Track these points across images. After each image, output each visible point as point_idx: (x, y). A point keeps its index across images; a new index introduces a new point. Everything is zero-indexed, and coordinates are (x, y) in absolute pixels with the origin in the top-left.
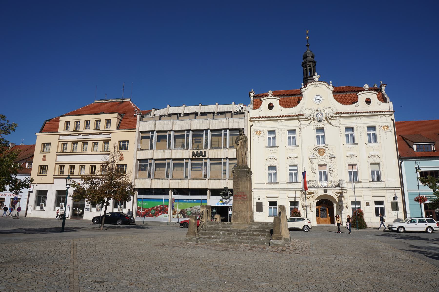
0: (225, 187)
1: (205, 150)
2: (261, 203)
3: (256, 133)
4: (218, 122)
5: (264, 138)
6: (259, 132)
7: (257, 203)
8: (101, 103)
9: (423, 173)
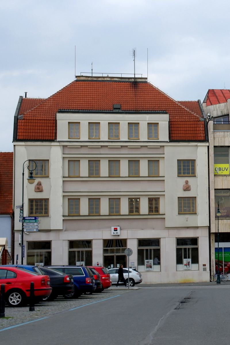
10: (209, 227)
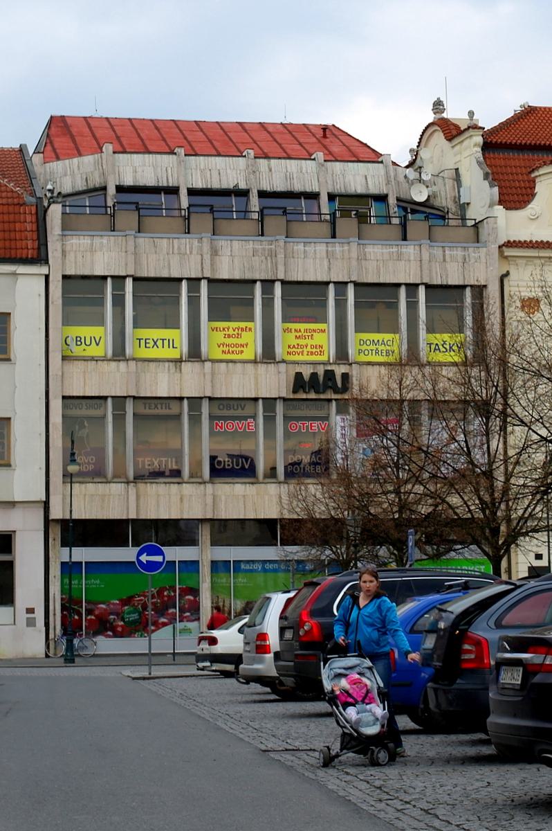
4: (386, 257)
9: (261, 640)
10: (46, 505)
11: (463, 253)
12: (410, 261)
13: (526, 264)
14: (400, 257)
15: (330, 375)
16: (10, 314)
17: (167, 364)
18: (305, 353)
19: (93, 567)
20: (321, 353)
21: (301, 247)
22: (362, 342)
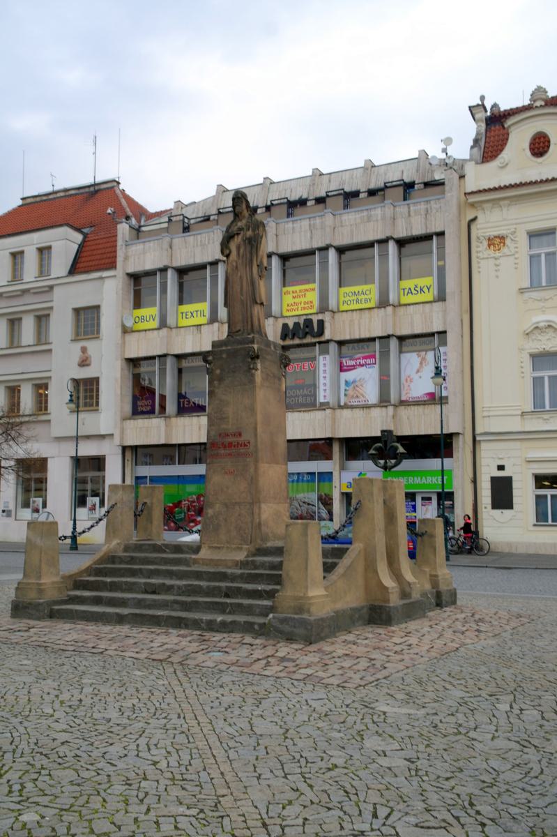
0: (383, 432)
1: (320, 317)
2: (509, 480)
3: (489, 245)
5: (516, 259)
6: (497, 242)
7: (494, 480)
8: (45, 201)
11: (426, 206)
12: (377, 220)
13: (509, 205)
14: (369, 219)
15: (308, 323)
16: (98, 307)
17: (191, 328)
18: (300, 309)
19: (154, 479)
20: (312, 307)
21: (290, 225)
22: (345, 295)
